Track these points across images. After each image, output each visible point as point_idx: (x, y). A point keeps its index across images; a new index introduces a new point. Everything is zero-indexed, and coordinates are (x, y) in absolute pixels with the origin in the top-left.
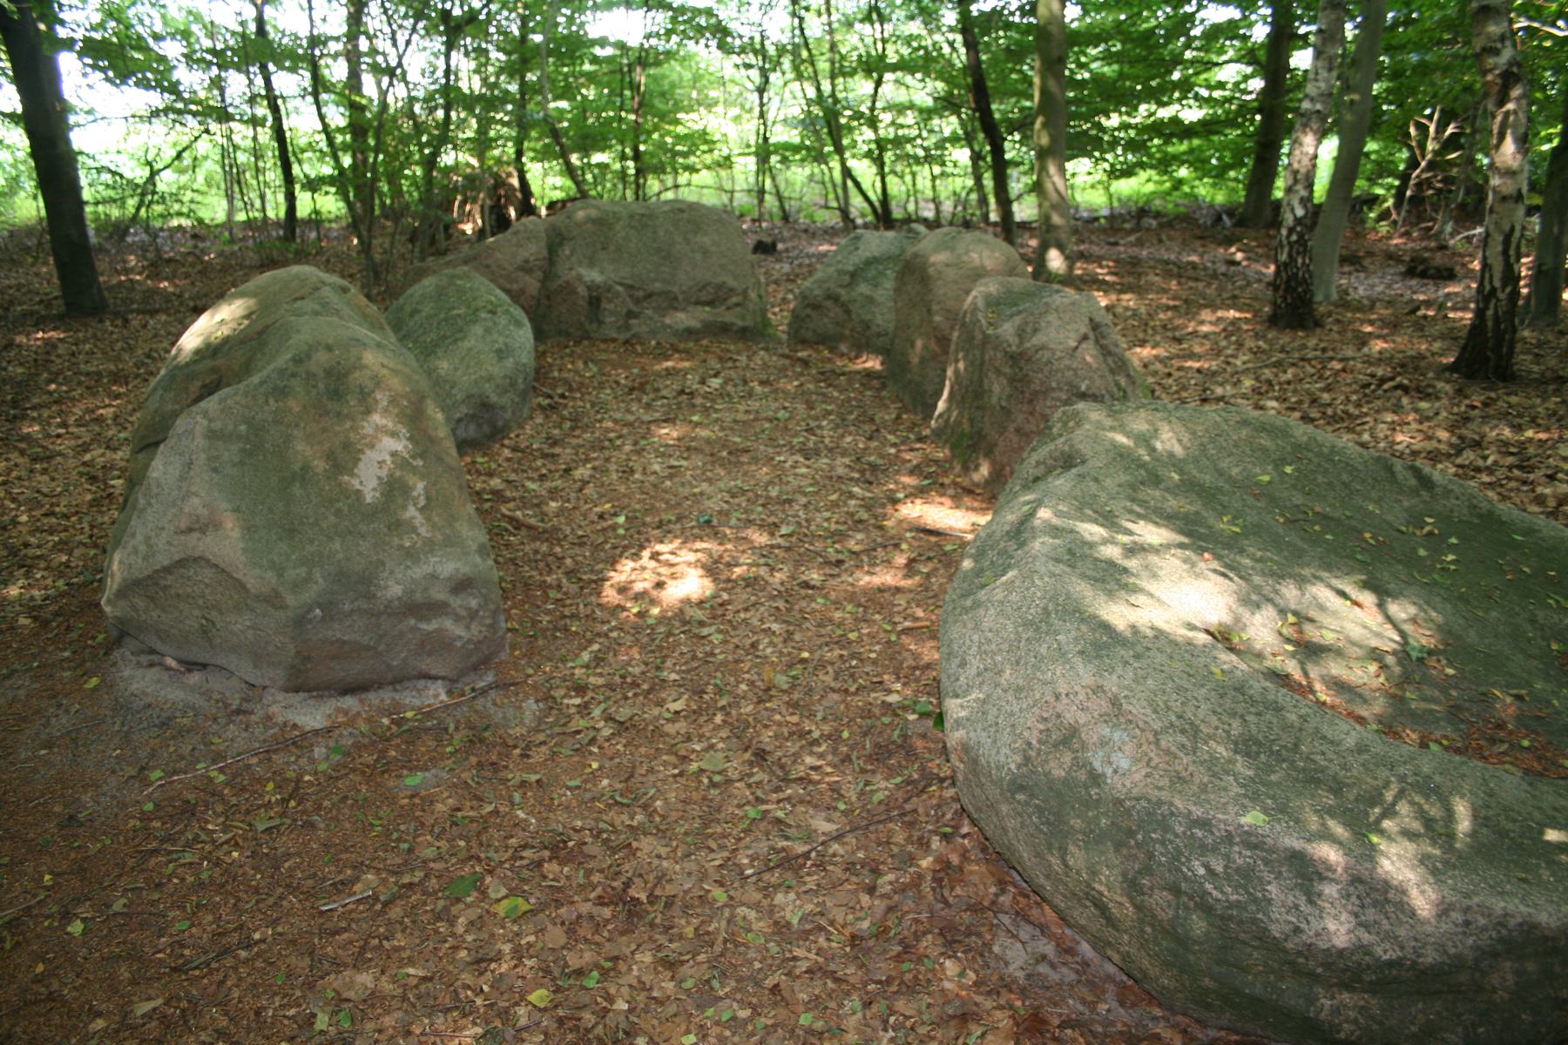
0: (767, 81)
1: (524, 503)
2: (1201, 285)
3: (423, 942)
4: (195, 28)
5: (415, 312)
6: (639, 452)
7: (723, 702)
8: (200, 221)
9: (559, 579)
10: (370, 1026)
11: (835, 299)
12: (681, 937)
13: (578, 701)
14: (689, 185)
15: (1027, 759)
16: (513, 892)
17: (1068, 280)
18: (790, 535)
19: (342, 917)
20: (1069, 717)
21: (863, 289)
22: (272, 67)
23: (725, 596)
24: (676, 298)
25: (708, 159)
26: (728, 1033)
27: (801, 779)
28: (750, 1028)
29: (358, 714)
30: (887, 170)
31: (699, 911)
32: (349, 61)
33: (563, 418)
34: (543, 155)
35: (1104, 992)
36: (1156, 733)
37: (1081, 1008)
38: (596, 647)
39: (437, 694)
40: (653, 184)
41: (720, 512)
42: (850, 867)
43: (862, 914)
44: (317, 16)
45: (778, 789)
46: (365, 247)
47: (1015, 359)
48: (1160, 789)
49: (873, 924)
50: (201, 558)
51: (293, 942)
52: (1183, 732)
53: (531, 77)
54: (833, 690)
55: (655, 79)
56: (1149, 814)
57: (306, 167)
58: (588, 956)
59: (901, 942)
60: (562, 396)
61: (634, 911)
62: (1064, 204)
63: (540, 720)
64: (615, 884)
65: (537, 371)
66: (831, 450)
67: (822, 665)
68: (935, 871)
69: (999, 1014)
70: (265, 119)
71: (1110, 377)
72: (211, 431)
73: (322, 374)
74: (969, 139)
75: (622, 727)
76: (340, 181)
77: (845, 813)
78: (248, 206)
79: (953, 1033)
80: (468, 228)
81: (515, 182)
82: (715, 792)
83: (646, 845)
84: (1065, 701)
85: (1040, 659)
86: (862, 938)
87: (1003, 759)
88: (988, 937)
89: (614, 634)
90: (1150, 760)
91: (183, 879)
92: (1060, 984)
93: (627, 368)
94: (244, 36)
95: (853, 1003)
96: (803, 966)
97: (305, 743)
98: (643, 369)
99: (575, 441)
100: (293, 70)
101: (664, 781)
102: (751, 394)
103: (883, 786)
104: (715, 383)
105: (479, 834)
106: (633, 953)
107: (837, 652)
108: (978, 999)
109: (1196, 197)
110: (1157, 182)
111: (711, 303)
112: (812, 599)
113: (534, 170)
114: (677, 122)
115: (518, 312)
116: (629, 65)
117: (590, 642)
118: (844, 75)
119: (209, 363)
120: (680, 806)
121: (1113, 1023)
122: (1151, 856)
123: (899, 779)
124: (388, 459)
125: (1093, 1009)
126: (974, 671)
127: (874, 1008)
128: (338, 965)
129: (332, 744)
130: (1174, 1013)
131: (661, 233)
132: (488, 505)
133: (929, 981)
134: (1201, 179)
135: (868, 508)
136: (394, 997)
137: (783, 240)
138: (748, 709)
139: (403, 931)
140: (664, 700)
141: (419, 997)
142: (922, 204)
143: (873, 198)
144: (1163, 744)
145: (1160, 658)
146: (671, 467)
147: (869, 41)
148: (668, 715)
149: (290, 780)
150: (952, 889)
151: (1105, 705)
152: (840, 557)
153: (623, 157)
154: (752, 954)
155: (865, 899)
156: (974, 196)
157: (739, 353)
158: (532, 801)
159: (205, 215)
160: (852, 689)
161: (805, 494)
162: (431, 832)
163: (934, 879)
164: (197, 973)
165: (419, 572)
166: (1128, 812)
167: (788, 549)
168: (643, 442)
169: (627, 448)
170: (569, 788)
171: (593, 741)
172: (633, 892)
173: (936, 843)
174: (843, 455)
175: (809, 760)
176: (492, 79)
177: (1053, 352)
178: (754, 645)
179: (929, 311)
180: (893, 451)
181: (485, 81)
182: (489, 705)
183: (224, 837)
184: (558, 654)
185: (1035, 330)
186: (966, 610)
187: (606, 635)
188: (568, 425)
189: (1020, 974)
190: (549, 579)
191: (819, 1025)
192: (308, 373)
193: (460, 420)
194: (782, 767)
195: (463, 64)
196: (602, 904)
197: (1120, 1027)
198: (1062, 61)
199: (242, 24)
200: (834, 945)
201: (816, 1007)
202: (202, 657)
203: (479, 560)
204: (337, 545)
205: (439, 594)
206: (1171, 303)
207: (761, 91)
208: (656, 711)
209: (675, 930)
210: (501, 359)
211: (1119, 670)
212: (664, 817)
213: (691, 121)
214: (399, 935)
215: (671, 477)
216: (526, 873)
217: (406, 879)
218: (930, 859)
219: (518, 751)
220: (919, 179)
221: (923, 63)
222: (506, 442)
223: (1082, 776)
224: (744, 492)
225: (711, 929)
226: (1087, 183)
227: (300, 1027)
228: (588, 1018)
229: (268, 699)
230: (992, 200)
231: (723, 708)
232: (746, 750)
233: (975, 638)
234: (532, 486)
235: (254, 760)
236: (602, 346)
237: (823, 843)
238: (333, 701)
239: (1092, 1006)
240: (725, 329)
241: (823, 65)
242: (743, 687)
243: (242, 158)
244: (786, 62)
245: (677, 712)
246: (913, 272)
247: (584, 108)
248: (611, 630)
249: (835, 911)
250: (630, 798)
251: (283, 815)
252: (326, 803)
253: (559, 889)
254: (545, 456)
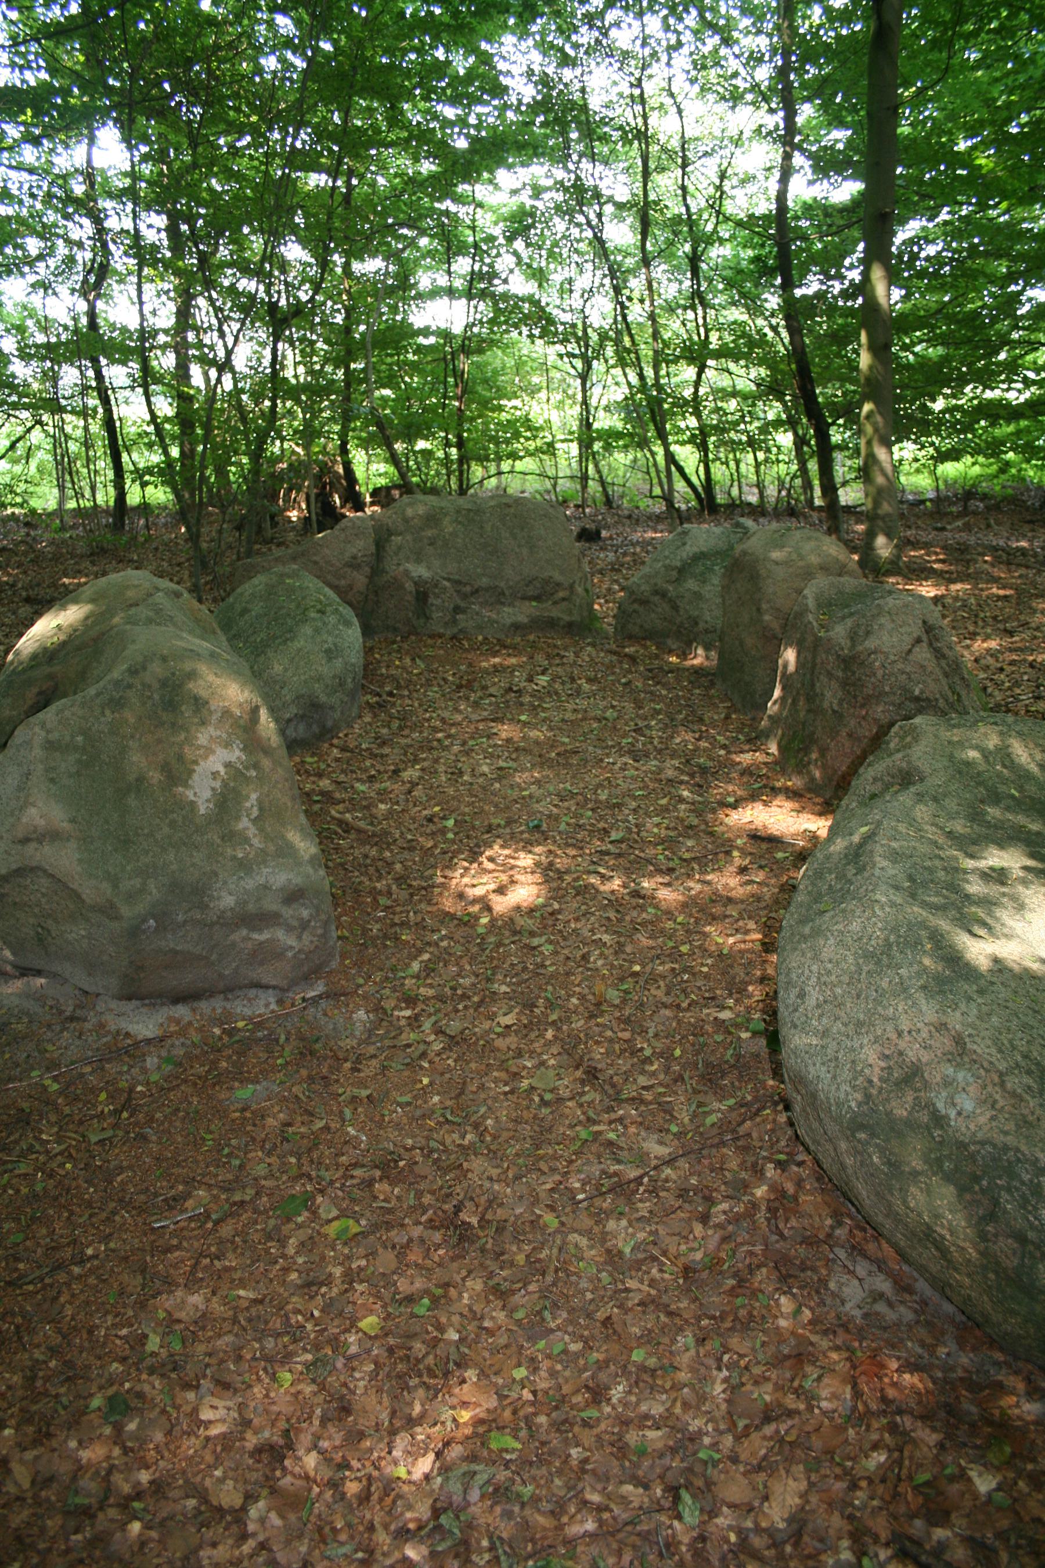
0: (590, 367)
1: (353, 805)
2: (1031, 573)
3: (253, 1262)
4: (30, 323)
5: (245, 611)
6: (467, 753)
7: (554, 1017)
8: (33, 512)
9: (389, 886)
10: (201, 1348)
11: (663, 594)
12: (512, 1264)
13: (408, 1013)
14: (511, 472)
15: (868, 1096)
16: (343, 1214)
17: (894, 567)
18: (620, 841)
19: (174, 1234)
20: (911, 1056)
21: (691, 584)
22: (103, 361)
23: (556, 906)
25: (532, 445)
26: (559, 1367)
27: (633, 1099)
28: (582, 1362)
29: (190, 1023)
30: (711, 456)
31: (530, 1236)
32: (177, 353)
33: (391, 717)
34: (365, 444)
35: (943, 1333)
36: (1001, 1075)
37: (920, 1351)
38: (426, 957)
39: (264, 1005)
40: (477, 471)
41: (549, 816)
42: (682, 1193)
43: (696, 1245)
44: (147, 309)
45: (610, 1109)
46: (193, 537)
47: (849, 662)
48: (1006, 1133)
49: (705, 1255)
50: (38, 868)
51: (126, 1259)
52: (1029, 1072)
53: (357, 366)
54: (665, 1006)
55: (478, 366)
56: (994, 1159)
57: (135, 456)
58: (419, 1284)
59: (735, 1275)
60: (390, 694)
61: (464, 1235)
62: (890, 490)
63: (370, 1032)
64: (446, 1207)
65: (366, 667)
66: (660, 752)
67: (653, 978)
68: (769, 1200)
69: (834, 1356)
70: (95, 410)
71: (944, 681)
72: (48, 742)
73: (156, 685)
74: (792, 423)
75: (453, 1041)
76: (166, 473)
77: (678, 1135)
78: (79, 495)
79: (788, 1375)
80: (293, 515)
81: (340, 470)
82: (545, 1111)
83: (477, 1165)
84: (908, 1038)
85: (881, 993)
86: (695, 1271)
87: (842, 1096)
88: (824, 1272)
89: (444, 944)
90: (995, 1102)
91: (18, 1191)
92: (898, 1324)
93: (455, 664)
94: (76, 331)
95: (686, 1339)
96: (636, 1298)
97: (138, 1053)
98: (470, 665)
99: (404, 741)
100: (124, 363)
101: (495, 1099)
102: (578, 692)
103: (718, 1109)
104: (543, 680)
105: (310, 1150)
106: (463, 1279)
107: (667, 966)
108: (814, 1338)
109: (1023, 479)
110: (982, 465)
111: (537, 598)
112: (643, 908)
113: (358, 457)
114: (500, 409)
115: (347, 612)
116: (452, 353)
117: (420, 952)
118: (668, 363)
119: (47, 670)
120: (511, 1125)
121: (952, 1369)
122: (996, 1203)
123: (732, 1102)
124: (222, 770)
125: (932, 1353)
126: (813, 1002)
127: (708, 1345)
128: (170, 1284)
129: (164, 1053)
130: (1016, 1358)
131: (488, 528)
132: (317, 809)
133: (763, 1317)
134: (1028, 461)
135: (699, 814)
136: (224, 1319)
137: (607, 527)
138: (579, 1024)
139: (234, 1251)
140: (495, 1014)
141: (250, 1320)
142: (745, 489)
143: (694, 480)
144: (1009, 1085)
145: (1004, 994)
146: (500, 769)
147: (691, 326)
148: (498, 1030)
149: (122, 1090)
150: (787, 1220)
151: (948, 1044)
152: (671, 865)
153: (448, 444)
154: (584, 1284)
155: (698, 1229)
156: (798, 482)
157: (566, 649)
158: (362, 1118)
159: (35, 503)
160: (684, 1005)
161: (635, 798)
162: (262, 1148)
163: (769, 1209)
164: (31, 1288)
165: (250, 884)
166: (972, 1157)
167: (619, 855)
168: (471, 743)
169: (456, 748)
170: (399, 1104)
171: (423, 1055)
172: (464, 1216)
173: (770, 1170)
174: (672, 757)
175: (643, 1081)
176: (317, 367)
177: (886, 655)
178: (585, 957)
179: (758, 610)
180: (722, 752)
181: (310, 372)
182: (319, 1015)
183: (57, 1148)
184: (388, 964)
185: (868, 633)
186: (805, 938)
187: (437, 945)
188: (396, 724)
189: (857, 1313)
190: (378, 885)
191: (652, 1362)
192: (143, 684)
193: (289, 721)
194: (613, 1086)
195: (290, 355)
196: (435, 1228)
197: (960, 1373)
198: (887, 346)
199: (74, 319)
200: (666, 1276)
201: (649, 1342)
202: (38, 964)
203: (311, 871)
204: (171, 856)
205: (271, 904)
206: (1001, 592)
207: (584, 377)
208: (487, 1025)
209: (505, 1257)
210: (330, 660)
211: (963, 1006)
212: (495, 1137)
213: (512, 407)
214: (230, 1255)
215: (499, 779)
216: (357, 1193)
217: (237, 1197)
218: (765, 1188)
219: (348, 1065)
220: (742, 466)
221: (747, 347)
222: (335, 741)
223: (924, 1117)
224: (573, 795)
225: (542, 1256)
226: (914, 466)
227: (132, 1348)
228: (419, 1347)
229: (101, 1007)
230: (816, 483)
231: (554, 1022)
232: (577, 1068)
233: (815, 968)
234: (360, 787)
235: (88, 1069)
236: (430, 641)
237: (655, 1168)
238: (165, 1009)
239: (931, 1349)
240: (551, 624)
241: (646, 352)
242: (574, 1001)
243: (73, 447)
244: (610, 351)
245: (507, 1027)
246: (742, 571)
247: (406, 397)
248: (442, 939)
249: (668, 1240)
250: (462, 1110)
251: (115, 1126)
252: (158, 1115)
253: (390, 1211)
254: (373, 756)
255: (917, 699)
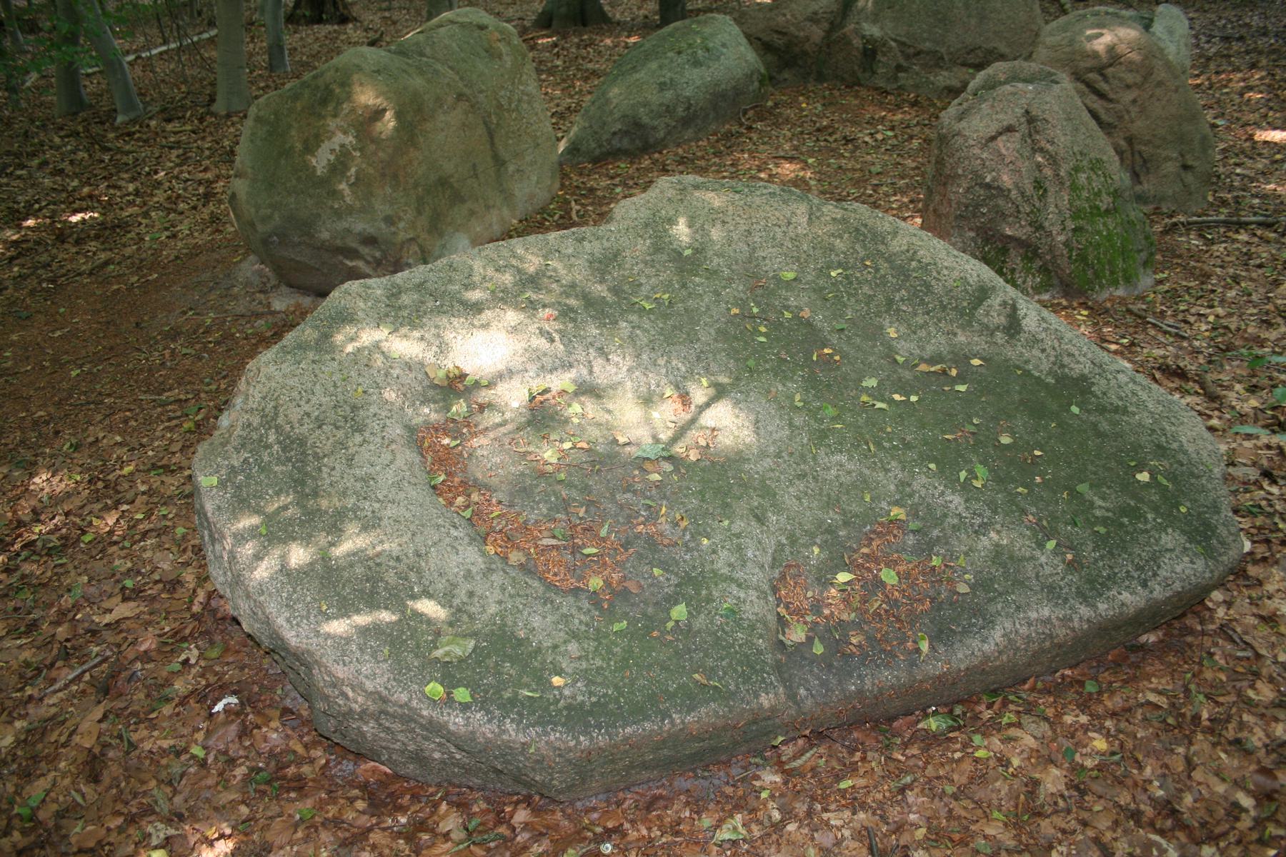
24: (942, 58)
124: (338, 148)
177: (966, 138)
193: (614, 133)
203: (383, 226)
255: (988, 186)
